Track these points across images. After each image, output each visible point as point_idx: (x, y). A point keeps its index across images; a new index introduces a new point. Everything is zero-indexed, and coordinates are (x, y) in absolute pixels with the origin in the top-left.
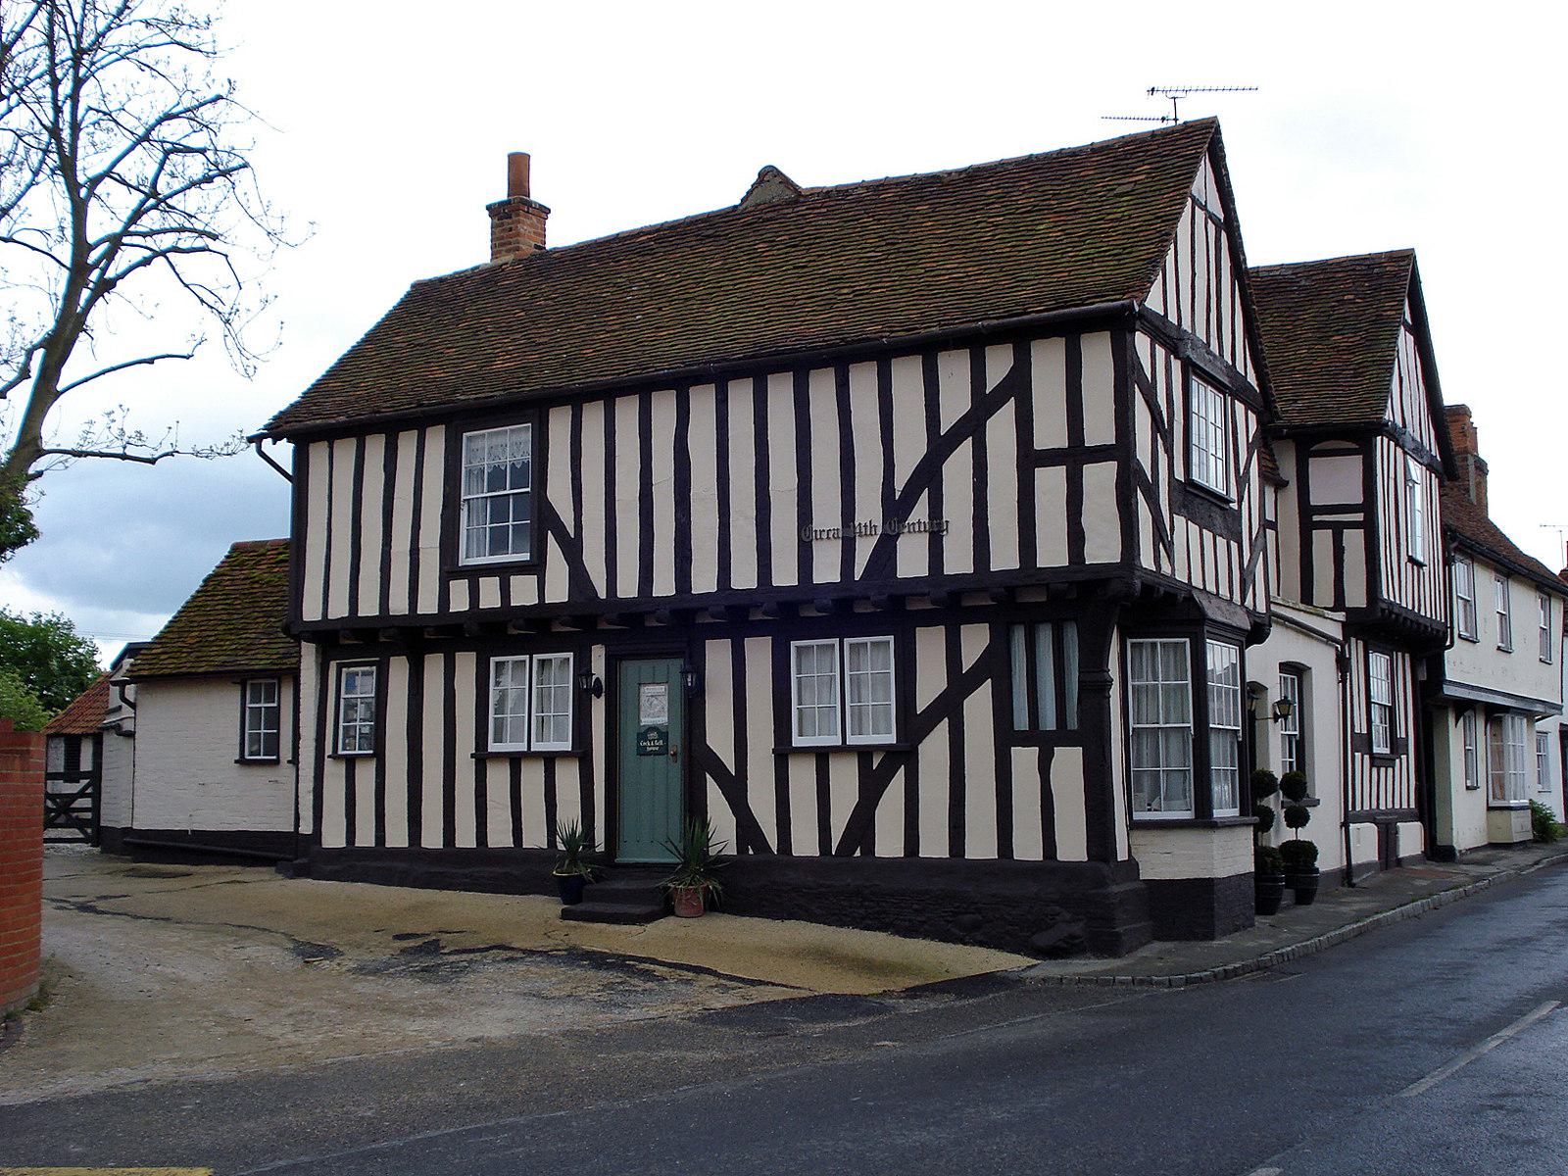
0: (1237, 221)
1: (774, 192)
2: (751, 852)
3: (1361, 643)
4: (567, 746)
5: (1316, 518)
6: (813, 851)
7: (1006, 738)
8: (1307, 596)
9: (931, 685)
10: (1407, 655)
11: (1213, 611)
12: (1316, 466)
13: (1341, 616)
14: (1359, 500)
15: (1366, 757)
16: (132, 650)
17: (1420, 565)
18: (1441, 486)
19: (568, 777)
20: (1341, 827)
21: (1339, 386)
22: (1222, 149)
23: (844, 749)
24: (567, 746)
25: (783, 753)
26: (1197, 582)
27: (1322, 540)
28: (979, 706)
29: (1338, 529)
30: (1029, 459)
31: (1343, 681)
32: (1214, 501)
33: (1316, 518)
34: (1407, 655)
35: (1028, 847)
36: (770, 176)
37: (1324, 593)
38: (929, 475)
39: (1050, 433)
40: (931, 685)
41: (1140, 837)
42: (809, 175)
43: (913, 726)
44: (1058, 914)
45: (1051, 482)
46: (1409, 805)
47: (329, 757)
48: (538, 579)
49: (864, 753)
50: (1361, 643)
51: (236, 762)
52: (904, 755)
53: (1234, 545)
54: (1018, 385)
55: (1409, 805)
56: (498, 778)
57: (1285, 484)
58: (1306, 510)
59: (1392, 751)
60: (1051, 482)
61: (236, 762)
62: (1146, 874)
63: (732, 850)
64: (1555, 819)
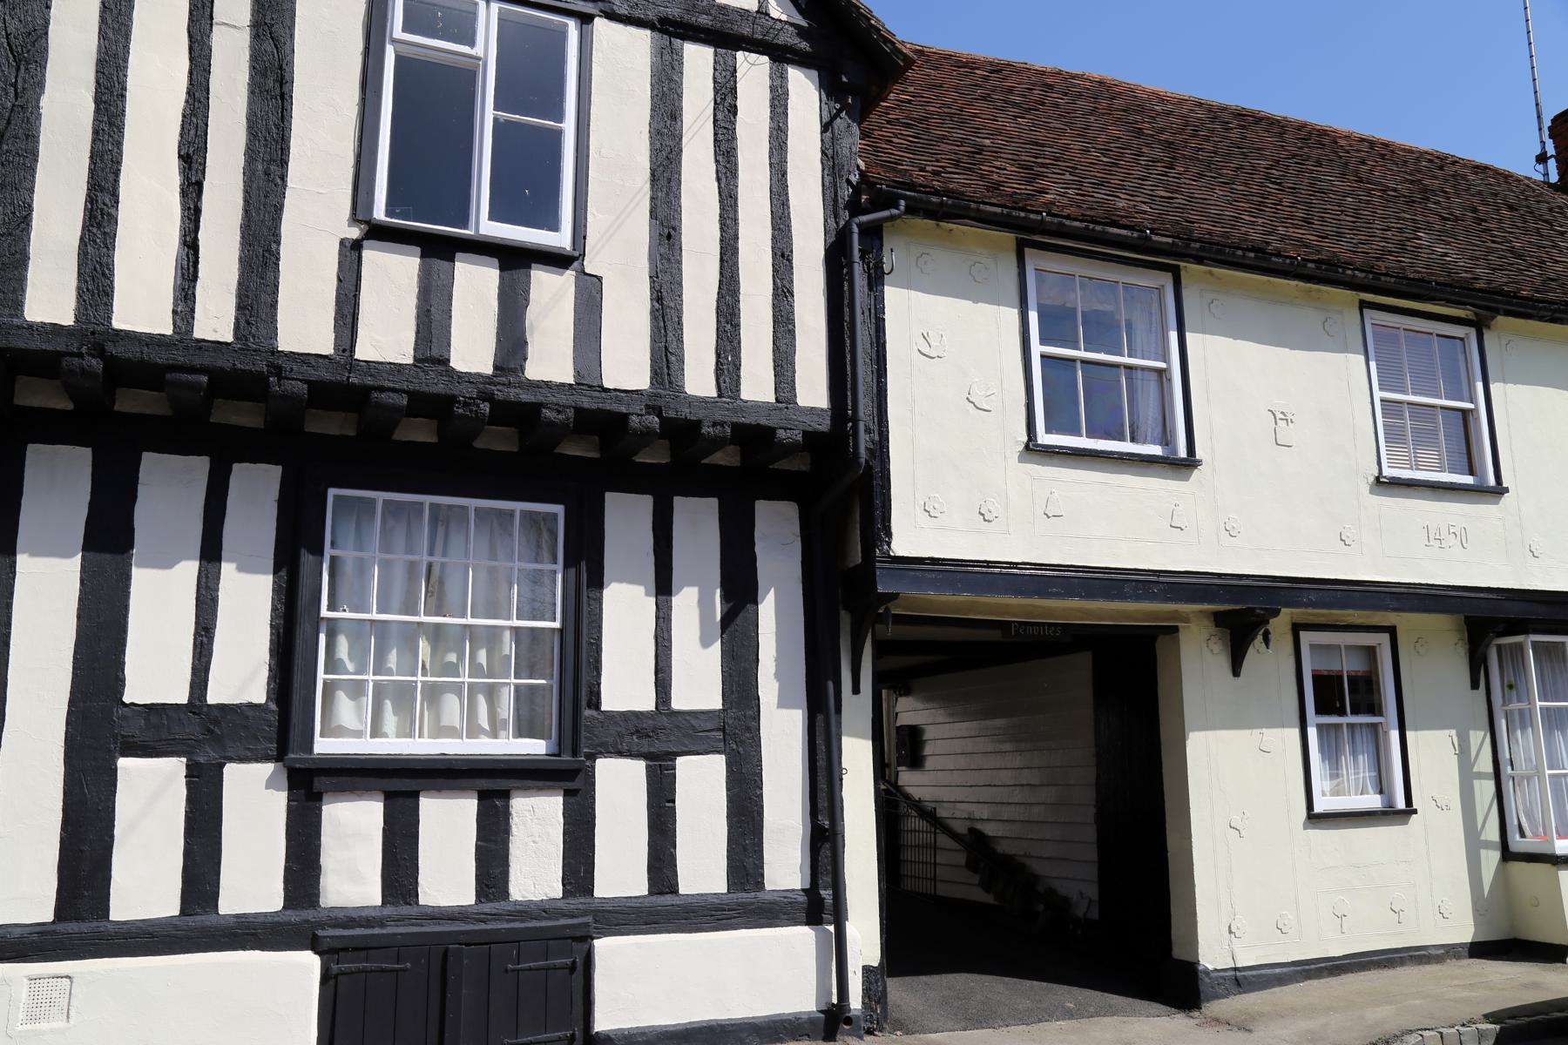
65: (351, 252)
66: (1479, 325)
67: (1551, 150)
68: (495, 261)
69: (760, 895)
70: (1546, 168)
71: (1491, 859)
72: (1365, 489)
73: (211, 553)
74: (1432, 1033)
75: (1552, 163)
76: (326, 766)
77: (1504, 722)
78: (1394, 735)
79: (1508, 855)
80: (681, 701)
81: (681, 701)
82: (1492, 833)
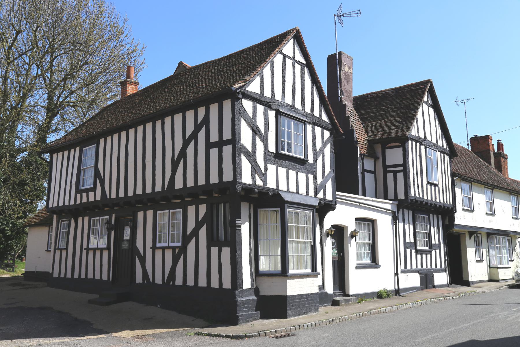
0: (435, 93)
2: (146, 282)
3: (410, 212)
4: (105, 246)
5: (388, 169)
6: (161, 283)
7: (210, 244)
9: (191, 225)
10: (440, 217)
11: (287, 198)
12: (388, 152)
13: (396, 202)
14: (401, 162)
15: (413, 251)
16: (333, 226)
18: (450, 159)
19: (105, 254)
21: (397, 125)
22: (302, 39)
23: (169, 247)
24: (105, 246)
25: (154, 248)
26: (283, 187)
27: (390, 176)
28: (203, 232)
29: (395, 173)
30: (209, 146)
33: (388, 169)
34: (228, 206)
35: (215, 284)
38: (183, 154)
39: (214, 137)
40: (191, 225)
42: (190, 63)
43: (186, 239)
45: (214, 152)
46: (417, 267)
47: (85, 249)
48: (94, 193)
49: (174, 248)
51: (46, 251)
52: (183, 249)
53: (311, 177)
54: (206, 120)
55: (417, 267)
56: (159, 254)
57: (378, 158)
58: (385, 167)
59: (430, 248)
60: (214, 152)
61: (46, 251)
63: (141, 282)
65: (427, 185)
66: (493, 189)
67: (470, 143)
68: (430, 185)
69: (316, 273)
70: (468, 147)
71: (489, 267)
72: (485, 214)
73: (409, 223)
74: (305, 324)
75: (470, 146)
76: (426, 250)
77: (418, 241)
78: (481, 249)
79: (490, 267)
80: (436, 243)
81: (436, 243)
82: (489, 265)
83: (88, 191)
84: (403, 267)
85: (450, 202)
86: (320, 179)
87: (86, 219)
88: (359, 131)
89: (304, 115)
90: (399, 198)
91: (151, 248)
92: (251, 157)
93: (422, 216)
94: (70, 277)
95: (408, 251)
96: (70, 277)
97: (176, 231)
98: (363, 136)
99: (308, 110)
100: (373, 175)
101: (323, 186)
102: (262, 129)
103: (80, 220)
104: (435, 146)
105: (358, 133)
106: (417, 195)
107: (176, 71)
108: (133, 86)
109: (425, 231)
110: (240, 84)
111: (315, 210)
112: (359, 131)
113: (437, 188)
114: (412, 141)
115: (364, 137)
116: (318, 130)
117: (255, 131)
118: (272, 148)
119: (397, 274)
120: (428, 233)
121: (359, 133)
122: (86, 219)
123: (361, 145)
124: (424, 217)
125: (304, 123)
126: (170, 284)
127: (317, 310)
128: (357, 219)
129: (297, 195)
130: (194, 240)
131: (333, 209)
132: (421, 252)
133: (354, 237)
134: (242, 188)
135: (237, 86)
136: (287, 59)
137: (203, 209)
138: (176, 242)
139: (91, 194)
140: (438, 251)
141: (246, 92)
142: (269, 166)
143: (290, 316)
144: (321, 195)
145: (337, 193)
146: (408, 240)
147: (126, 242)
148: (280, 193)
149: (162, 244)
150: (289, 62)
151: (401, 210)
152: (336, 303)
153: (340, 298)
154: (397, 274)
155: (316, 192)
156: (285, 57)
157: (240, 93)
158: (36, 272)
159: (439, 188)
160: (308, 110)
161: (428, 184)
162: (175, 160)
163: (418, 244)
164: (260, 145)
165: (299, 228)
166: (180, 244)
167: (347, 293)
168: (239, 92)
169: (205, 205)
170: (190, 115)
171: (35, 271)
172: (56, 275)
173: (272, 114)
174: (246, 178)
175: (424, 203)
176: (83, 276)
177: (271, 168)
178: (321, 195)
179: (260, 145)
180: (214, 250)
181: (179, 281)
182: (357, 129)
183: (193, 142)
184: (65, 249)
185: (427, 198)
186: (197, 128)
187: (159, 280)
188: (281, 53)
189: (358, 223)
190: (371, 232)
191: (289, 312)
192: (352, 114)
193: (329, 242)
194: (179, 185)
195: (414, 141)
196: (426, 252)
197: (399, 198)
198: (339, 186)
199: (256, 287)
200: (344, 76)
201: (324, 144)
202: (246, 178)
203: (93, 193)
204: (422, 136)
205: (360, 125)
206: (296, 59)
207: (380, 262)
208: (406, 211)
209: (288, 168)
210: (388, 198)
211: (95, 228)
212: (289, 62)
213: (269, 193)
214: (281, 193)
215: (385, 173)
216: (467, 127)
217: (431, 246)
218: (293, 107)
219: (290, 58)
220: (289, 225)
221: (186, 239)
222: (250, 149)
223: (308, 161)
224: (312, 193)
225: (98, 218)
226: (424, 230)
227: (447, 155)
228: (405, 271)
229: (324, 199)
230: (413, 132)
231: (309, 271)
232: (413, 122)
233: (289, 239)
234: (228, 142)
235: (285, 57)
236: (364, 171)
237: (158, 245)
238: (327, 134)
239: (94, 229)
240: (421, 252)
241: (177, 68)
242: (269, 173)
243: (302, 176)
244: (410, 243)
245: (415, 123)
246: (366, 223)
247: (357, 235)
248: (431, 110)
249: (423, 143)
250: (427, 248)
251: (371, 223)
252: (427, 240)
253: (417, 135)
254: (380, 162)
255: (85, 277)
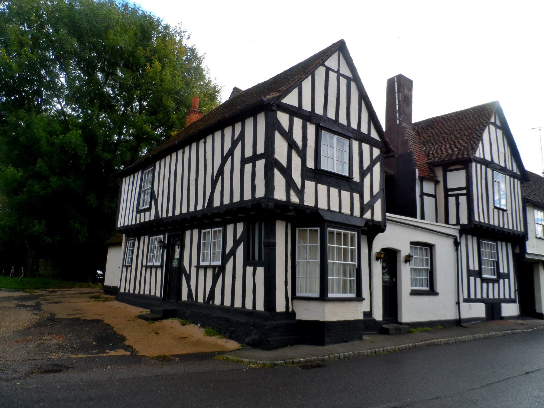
1: (237, 94)
2: (190, 300)
5: (450, 193)
6: (202, 301)
7: (246, 263)
8: (447, 221)
9: (230, 244)
13: (458, 227)
15: (478, 280)
16: (384, 250)
17: (504, 210)
19: (159, 271)
20: (51, 314)
25: (198, 267)
27: (452, 201)
29: (457, 196)
30: (244, 161)
31: (457, 250)
32: (344, 179)
33: (450, 193)
36: (236, 90)
37: (452, 219)
38: (221, 171)
40: (230, 244)
41: (296, 303)
42: (244, 87)
43: (225, 258)
44: (253, 330)
45: (248, 167)
49: (214, 267)
50: (475, 239)
52: (222, 269)
53: (356, 196)
54: (242, 136)
58: (446, 190)
62: (299, 317)
63: (187, 300)
64: (105, 322)
83: (144, 211)
84: (466, 296)
85: (520, 228)
86: (367, 198)
87: (147, 237)
88: (418, 154)
89: (349, 131)
90: (461, 223)
91: (195, 267)
92: (286, 172)
93: (488, 244)
94: (138, 293)
95: (472, 278)
96: (138, 293)
97: (217, 250)
98: (423, 159)
99: (354, 125)
100: (433, 199)
101: (371, 205)
102: (299, 143)
103: (142, 238)
104: (503, 170)
105: (417, 156)
106: (482, 220)
107: (231, 96)
108: (197, 115)
109: (492, 258)
110: (274, 94)
111: (360, 230)
112: (418, 154)
113: (505, 213)
114: (476, 163)
115: (423, 160)
116: (366, 147)
117: (292, 145)
118: (310, 164)
119: (458, 303)
120: (496, 261)
121: (418, 155)
122: (147, 237)
123: (420, 168)
124: (491, 244)
125: (349, 138)
126: (210, 303)
127: (360, 338)
128: (412, 243)
129: (340, 215)
130: (231, 260)
131: (383, 230)
132: (488, 281)
133: (408, 262)
134: (274, 204)
135: (270, 96)
136: (331, 72)
137: (240, 227)
138: (217, 261)
139: (147, 214)
140: (507, 280)
141: (281, 104)
142: (307, 183)
143: (328, 343)
144: (368, 215)
145: (387, 214)
146: (471, 268)
147: (176, 261)
148: (319, 211)
149: (216, 262)
150: (333, 76)
151: (464, 236)
152: (384, 332)
153: (391, 326)
154: (458, 303)
155: (362, 212)
156: (328, 69)
157: (274, 105)
158: (112, 286)
159: (507, 214)
160: (354, 125)
161: (495, 209)
162: (214, 178)
163: (483, 272)
164: (296, 161)
165: (341, 249)
166: (219, 263)
167: (399, 320)
168: (273, 104)
169: (242, 223)
170: (228, 131)
171: (111, 286)
172: (122, 290)
173: (311, 129)
174: (280, 194)
175: (490, 229)
176: (127, 291)
177: (310, 185)
178: (368, 215)
179: (296, 161)
180: (249, 269)
181: (217, 301)
182: (416, 152)
183: (230, 159)
184: (130, 266)
185: (494, 224)
186: (234, 144)
187: (200, 300)
188: (324, 65)
189: (413, 247)
190: (429, 258)
191: (327, 340)
192: (412, 136)
193: (378, 267)
194: (217, 203)
195: (479, 163)
196: (493, 281)
197: (461, 223)
198: (388, 208)
199: (293, 310)
200: (403, 99)
201: (373, 162)
202: (280, 194)
203: (149, 212)
204: (488, 158)
205: (419, 148)
206: (341, 72)
207: (438, 291)
208: (470, 237)
209: (329, 185)
210: (450, 222)
211: (206, 252)
212: (333, 76)
213: (307, 211)
214: (320, 211)
215: (447, 196)
216: (542, 150)
217: (500, 276)
218: (336, 121)
219: (333, 71)
220: (329, 246)
221: (225, 258)
222: (285, 164)
223: (353, 180)
224: (357, 213)
225: (156, 237)
226: (490, 257)
227: (518, 179)
228: (468, 300)
229: (372, 220)
230: (478, 154)
231: (353, 295)
232: (478, 143)
233: (328, 261)
234: (261, 157)
235: (328, 69)
236: (423, 194)
237: (202, 264)
238: (376, 152)
239: (152, 247)
240: (488, 281)
241: (232, 93)
242: (306, 190)
243: (346, 195)
244: (474, 271)
245: (480, 145)
246: (417, 248)
247: (411, 259)
248: (500, 132)
249: (489, 165)
250: (494, 277)
251: (429, 249)
252: (494, 269)
253: (482, 157)
254: (441, 186)
255: (143, 293)
